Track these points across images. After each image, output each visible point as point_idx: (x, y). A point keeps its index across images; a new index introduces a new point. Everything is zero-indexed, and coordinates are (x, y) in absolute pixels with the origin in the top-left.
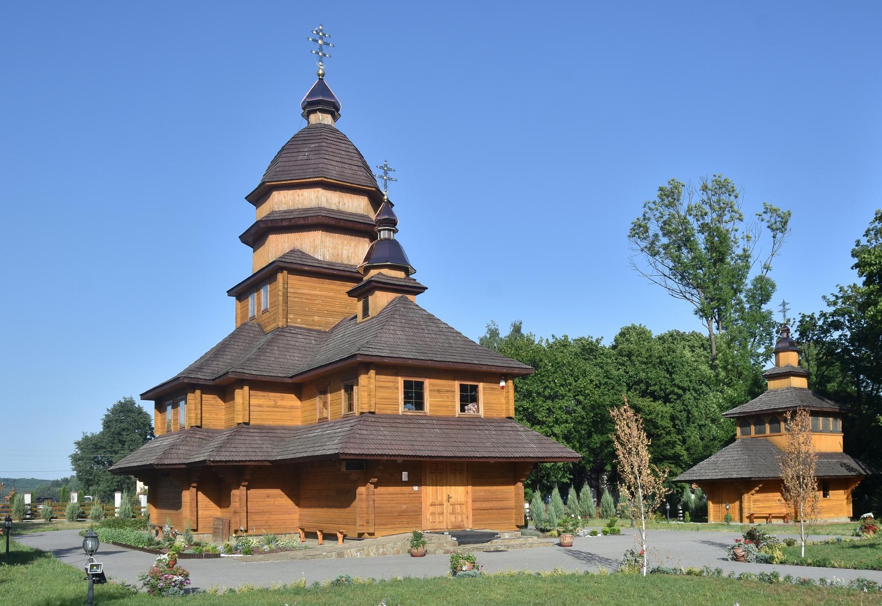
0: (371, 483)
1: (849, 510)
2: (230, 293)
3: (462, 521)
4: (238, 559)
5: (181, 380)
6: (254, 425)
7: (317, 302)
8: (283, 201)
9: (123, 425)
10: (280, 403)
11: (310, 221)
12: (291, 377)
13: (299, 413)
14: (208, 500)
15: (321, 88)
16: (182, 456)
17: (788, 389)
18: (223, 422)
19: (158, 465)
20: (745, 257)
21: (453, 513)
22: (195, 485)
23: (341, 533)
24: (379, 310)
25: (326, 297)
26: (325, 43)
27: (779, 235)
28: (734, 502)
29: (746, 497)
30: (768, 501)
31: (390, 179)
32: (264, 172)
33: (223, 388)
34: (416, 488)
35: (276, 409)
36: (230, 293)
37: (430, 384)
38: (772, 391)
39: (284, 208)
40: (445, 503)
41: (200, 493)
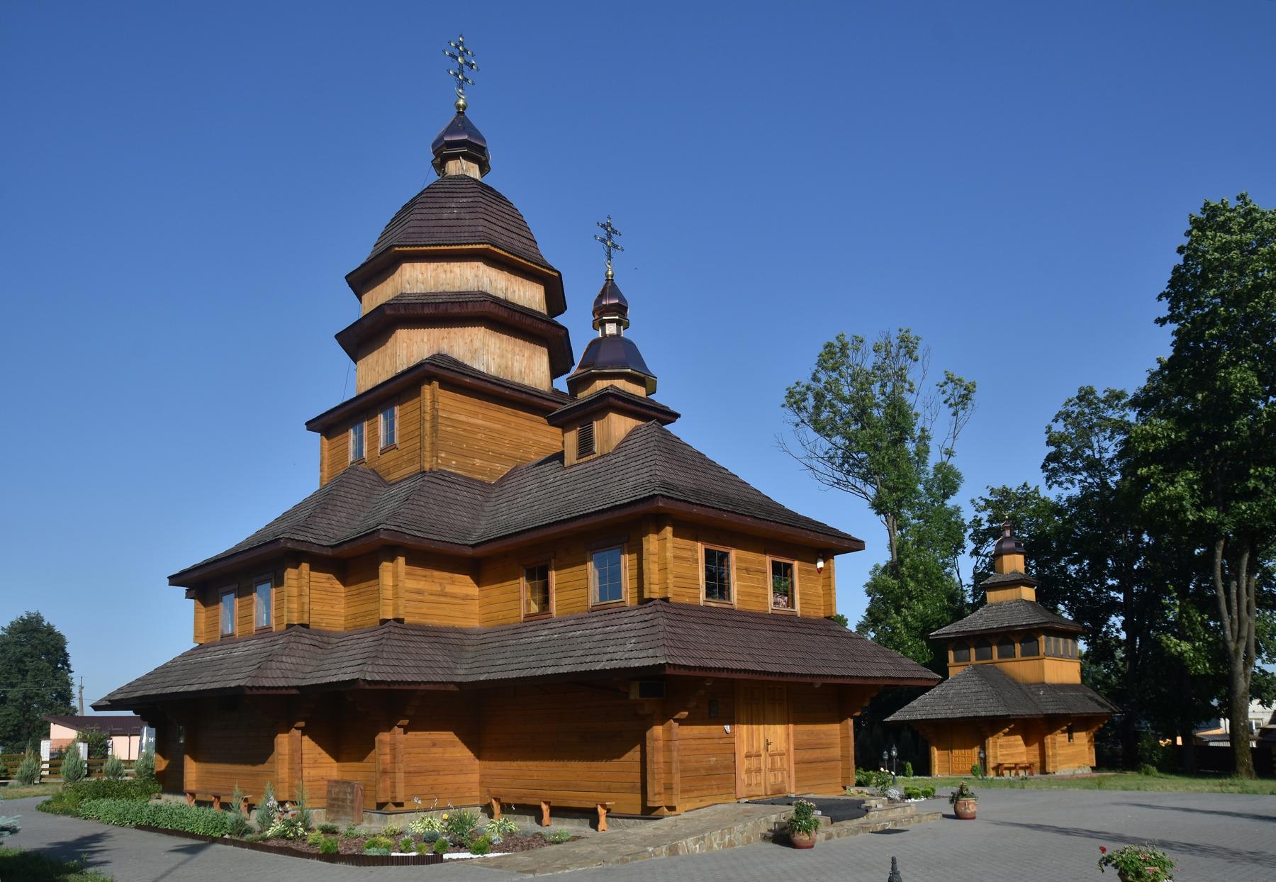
0: (297, 728)
1: (1090, 758)
2: (312, 425)
3: (783, 782)
4: (498, 864)
5: (282, 544)
6: (410, 624)
7: (479, 436)
8: (417, 279)
9: (27, 649)
10: (450, 589)
11: (470, 309)
12: (473, 546)
13: (475, 607)
14: (320, 750)
15: (461, 121)
16: (289, 674)
17: (1016, 601)
18: (342, 621)
19: (251, 688)
20: (924, 438)
21: (772, 770)
22: (302, 724)
23: (604, 806)
24: (615, 443)
25: (491, 430)
26: (467, 63)
27: (961, 413)
28: (971, 748)
29: (990, 741)
30: (1010, 746)
31: (615, 246)
32: (375, 241)
33: (353, 562)
34: (728, 728)
35: (443, 599)
36: (312, 425)
37: (739, 559)
38: (992, 605)
39: (420, 289)
40: (763, 753)
41: (306, 738)
